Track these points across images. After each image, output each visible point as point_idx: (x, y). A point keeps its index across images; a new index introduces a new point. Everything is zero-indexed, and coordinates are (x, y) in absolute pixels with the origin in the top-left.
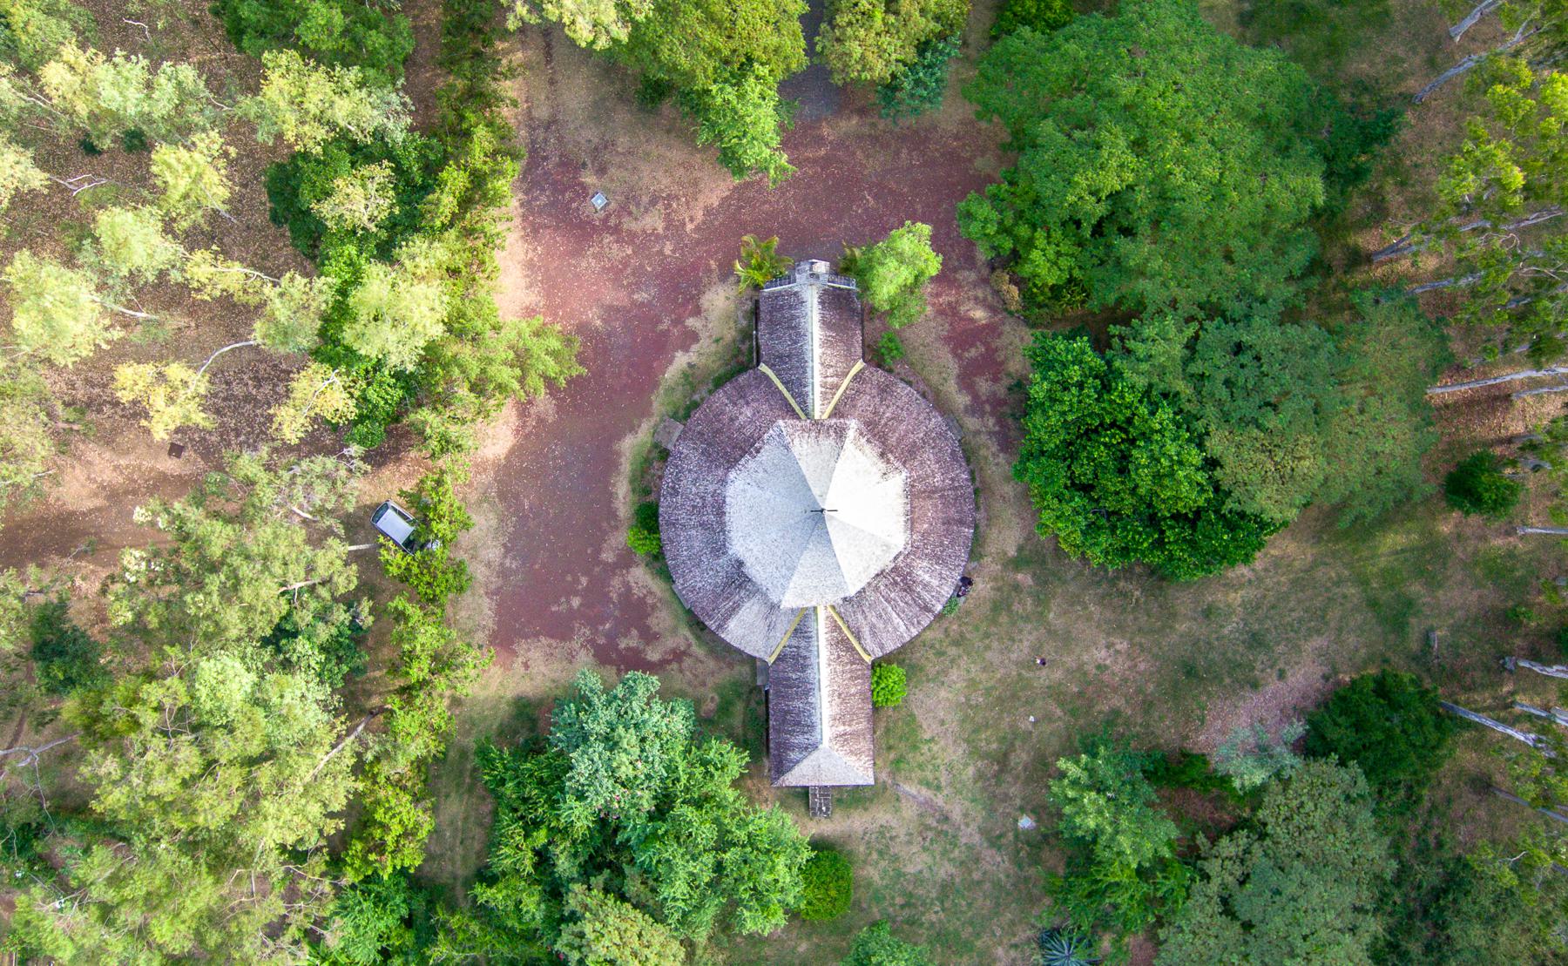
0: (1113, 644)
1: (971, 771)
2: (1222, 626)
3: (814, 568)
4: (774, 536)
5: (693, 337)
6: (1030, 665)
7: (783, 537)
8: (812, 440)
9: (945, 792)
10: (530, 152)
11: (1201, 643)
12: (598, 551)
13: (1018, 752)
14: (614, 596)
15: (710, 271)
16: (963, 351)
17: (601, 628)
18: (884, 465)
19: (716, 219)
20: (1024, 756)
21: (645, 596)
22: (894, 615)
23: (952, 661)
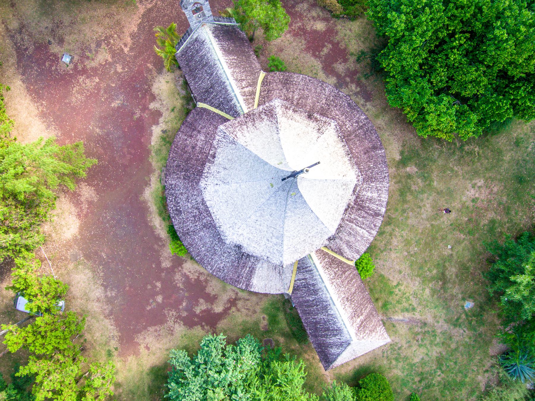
0: (475, 184)
1: (427, 291)
2: (527, 148)
3: (299, 228)
4: (254, 218)
5: (157, 114)
6: (435, 217)
7: (262, 216)
8: (251, 128)
9: (419, 310)
10: (16, 50)
11: (521, 162)
12: (159, 263)
13: (449, 269)
14: (180, 285)
15: (150, 70)
16: (319, 52)
17: (181, 307)
18: (315, 123)
19: (140, 38)
20: (454, 270)
21: (198, 277)
22: (358, 228)
23: (391, 235)
